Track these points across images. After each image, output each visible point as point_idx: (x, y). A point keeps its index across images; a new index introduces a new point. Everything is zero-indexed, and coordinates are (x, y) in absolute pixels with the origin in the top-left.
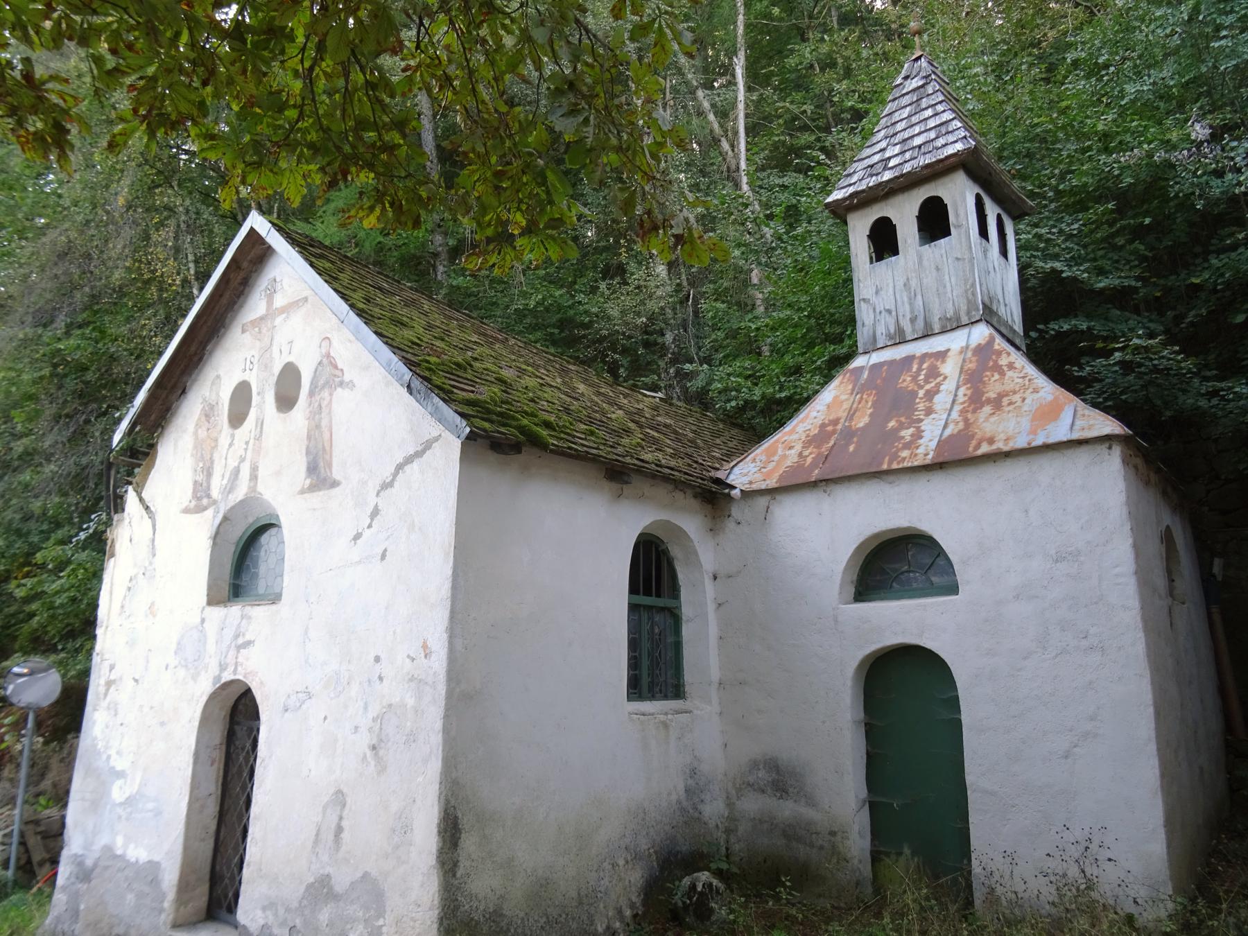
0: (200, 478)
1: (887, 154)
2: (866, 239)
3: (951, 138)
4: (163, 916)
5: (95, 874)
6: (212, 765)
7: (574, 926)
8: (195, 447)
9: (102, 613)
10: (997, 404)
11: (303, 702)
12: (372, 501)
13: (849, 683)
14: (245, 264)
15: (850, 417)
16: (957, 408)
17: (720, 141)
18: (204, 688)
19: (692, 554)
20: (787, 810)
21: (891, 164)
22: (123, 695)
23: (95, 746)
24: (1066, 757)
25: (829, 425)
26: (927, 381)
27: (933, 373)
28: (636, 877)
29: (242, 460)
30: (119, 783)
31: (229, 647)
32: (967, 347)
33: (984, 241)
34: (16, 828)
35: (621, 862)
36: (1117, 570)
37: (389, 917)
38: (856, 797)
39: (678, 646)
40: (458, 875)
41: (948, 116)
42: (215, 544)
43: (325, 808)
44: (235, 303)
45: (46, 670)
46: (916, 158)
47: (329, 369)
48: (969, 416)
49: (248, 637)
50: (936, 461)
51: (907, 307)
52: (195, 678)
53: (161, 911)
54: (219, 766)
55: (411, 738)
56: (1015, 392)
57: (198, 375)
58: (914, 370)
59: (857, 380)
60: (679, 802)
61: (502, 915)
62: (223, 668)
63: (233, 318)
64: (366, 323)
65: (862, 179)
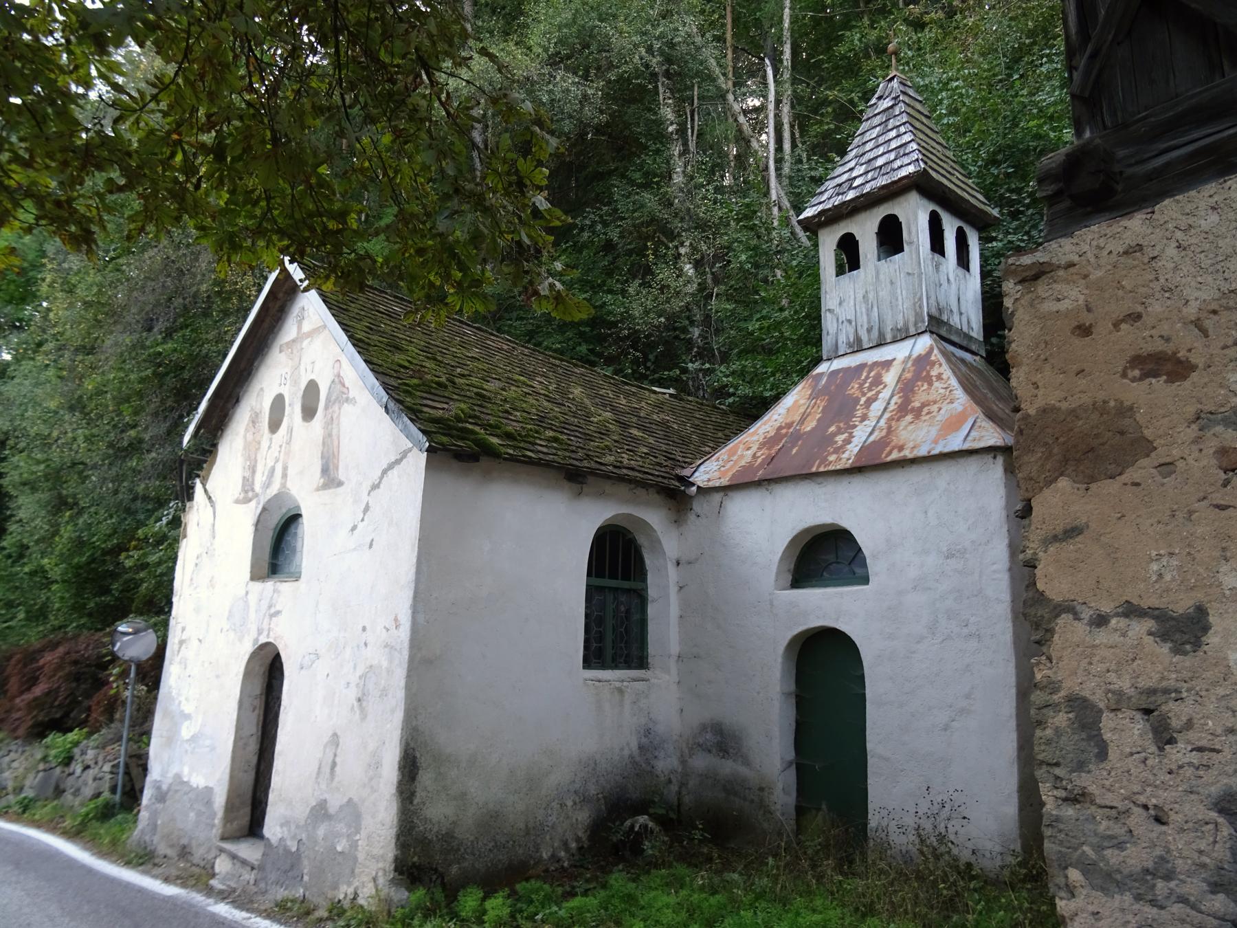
0: (247, 474)
1: (855, 174)
2: (875, 236)
3: (906, 160)
4: (214, 831)
5: (168, 797)
6: (254, 711)
7: (521, 851)
8: (245, 448)
9: (177, 584)
10: (918, 413)
11: (313, 662)
12: (365, 498)
13: (780, 660)
14: (281, 295)
15: (803, 420)
16: (887, 415)
17: (749, 141)
18: (247, 648)
19: (656, 543)
20: (728, 767)
21: (856, 184)
22: (189, 652)
23: (170, 693)
24: (946, 730)
25: (783, 428)
26: (870, 389)
27: (878, 381)
28: (583, 816)
29: (277, 460)
30: (186, 724)
31: (265, 615)
32: (910, 356)
33: (937, 256)
34: (122, 760)
35: (570, 803)
36: (995, 567)
37: (363, 834)
38: (782, 759)
39: (643, 623)
40: (415, 802)
41: (907, 138)
42: (256, 530)
43: (325, 747)
44: (275, 327)
45: (145, 630)
46: (876, 179)
47: (339, 386)
48: (893, 423)
49: (278, 608)
50: (854, 465)
51: (865, 317)
52: (241, 639)
53: (213, 826)
54: (260, 712)
55: (384, 693)
56: (935, 402)
57: (248, 386)
58: (863, 378)
59: (816, 385)
60: (631, 756)
61: (453, 837)
62: (260, 632)
63: (274, 339)
64: (359, 352)
65: (831, 197)
